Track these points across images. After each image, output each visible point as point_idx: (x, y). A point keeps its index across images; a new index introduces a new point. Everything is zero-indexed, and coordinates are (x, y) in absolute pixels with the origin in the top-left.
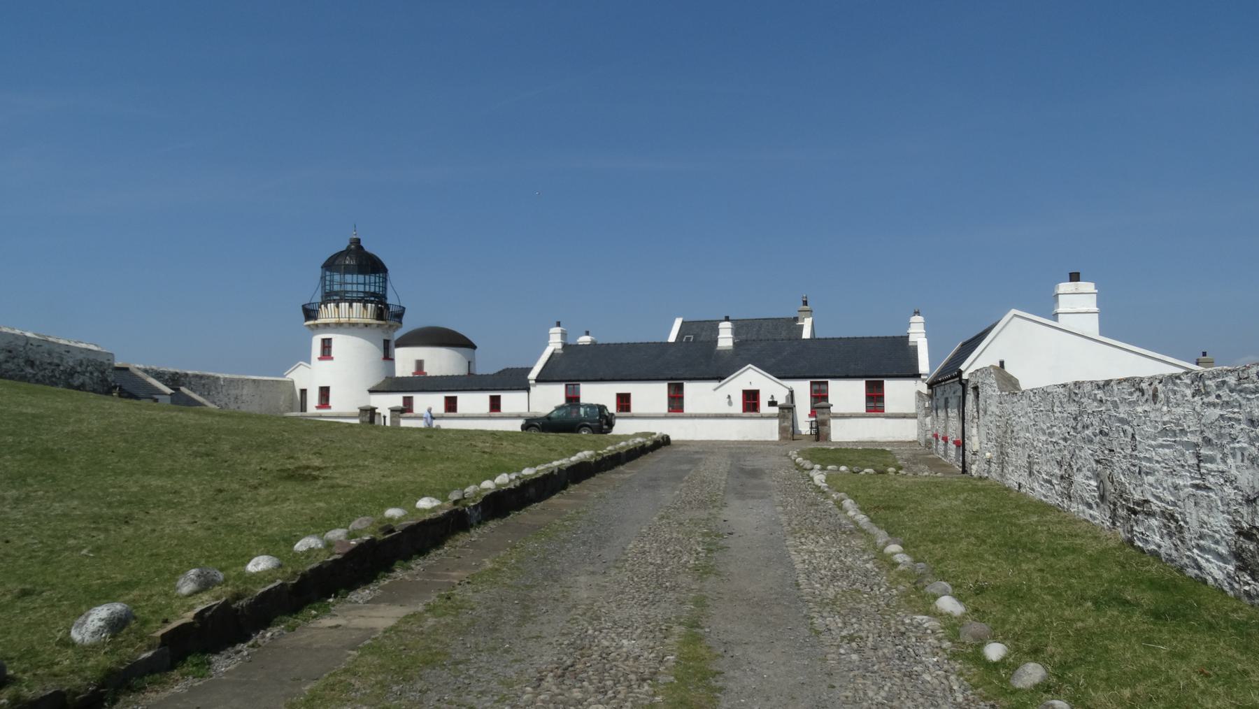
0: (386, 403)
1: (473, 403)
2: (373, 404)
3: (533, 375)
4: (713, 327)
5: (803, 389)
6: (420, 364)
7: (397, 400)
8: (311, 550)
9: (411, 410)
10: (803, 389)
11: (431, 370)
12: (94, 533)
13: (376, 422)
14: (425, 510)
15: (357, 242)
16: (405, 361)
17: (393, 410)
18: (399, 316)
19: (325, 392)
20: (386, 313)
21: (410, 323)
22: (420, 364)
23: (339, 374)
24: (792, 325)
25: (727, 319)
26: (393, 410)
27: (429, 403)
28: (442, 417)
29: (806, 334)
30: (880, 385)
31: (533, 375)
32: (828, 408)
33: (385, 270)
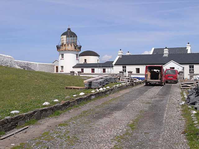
0: (77, 70)
1: (98, 71)
2: (74, 71)
3: (114, 63)
4: (162, 50)
5: (187, 67)
6: (85, 60)
7: (80, 70)
8: (57, 102)
9: (83, 72)
10: (187, 67)
11: (88, 62)
12: (33, 76)
13: (74, 75)
14: (32, 69)
15: (69, 29)
16: (82, 60)
17: (78, 72)
18: (80, 48)
19: (62, 67)
20: (78, 48)
21: (83, 50)
22: (85, 60)
23: (68, 63)
24: (185, 49)
25: (166, 48)
26: (78, 72)
27: (87, 71)
28: (90, 74)
29: (189, 52)
30: (193, 67)
31: (114, 63)
32: (193, 72)
33: (76, 37)
